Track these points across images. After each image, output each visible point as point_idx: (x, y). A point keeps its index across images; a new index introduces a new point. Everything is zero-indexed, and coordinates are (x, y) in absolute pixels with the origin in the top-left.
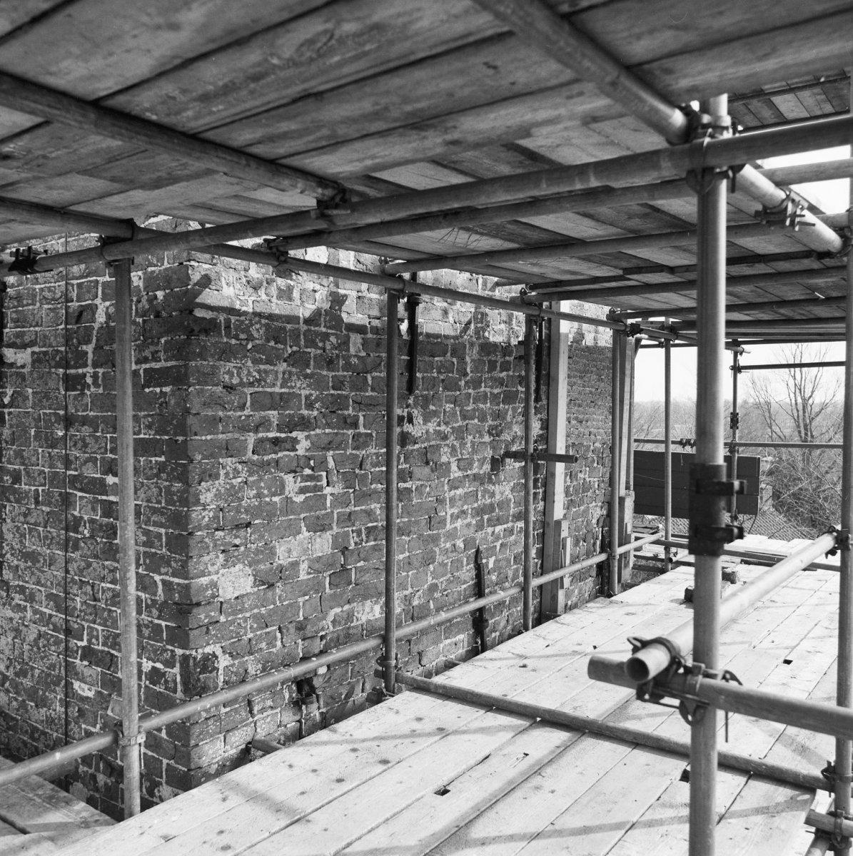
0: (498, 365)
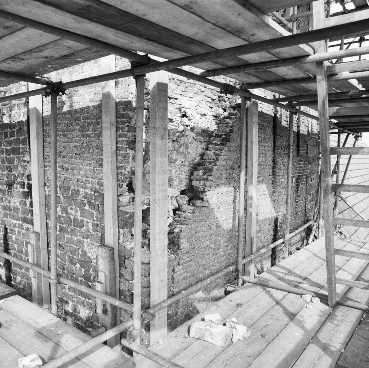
0: (8, 134)
